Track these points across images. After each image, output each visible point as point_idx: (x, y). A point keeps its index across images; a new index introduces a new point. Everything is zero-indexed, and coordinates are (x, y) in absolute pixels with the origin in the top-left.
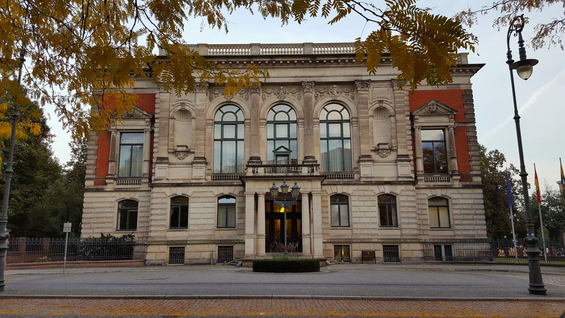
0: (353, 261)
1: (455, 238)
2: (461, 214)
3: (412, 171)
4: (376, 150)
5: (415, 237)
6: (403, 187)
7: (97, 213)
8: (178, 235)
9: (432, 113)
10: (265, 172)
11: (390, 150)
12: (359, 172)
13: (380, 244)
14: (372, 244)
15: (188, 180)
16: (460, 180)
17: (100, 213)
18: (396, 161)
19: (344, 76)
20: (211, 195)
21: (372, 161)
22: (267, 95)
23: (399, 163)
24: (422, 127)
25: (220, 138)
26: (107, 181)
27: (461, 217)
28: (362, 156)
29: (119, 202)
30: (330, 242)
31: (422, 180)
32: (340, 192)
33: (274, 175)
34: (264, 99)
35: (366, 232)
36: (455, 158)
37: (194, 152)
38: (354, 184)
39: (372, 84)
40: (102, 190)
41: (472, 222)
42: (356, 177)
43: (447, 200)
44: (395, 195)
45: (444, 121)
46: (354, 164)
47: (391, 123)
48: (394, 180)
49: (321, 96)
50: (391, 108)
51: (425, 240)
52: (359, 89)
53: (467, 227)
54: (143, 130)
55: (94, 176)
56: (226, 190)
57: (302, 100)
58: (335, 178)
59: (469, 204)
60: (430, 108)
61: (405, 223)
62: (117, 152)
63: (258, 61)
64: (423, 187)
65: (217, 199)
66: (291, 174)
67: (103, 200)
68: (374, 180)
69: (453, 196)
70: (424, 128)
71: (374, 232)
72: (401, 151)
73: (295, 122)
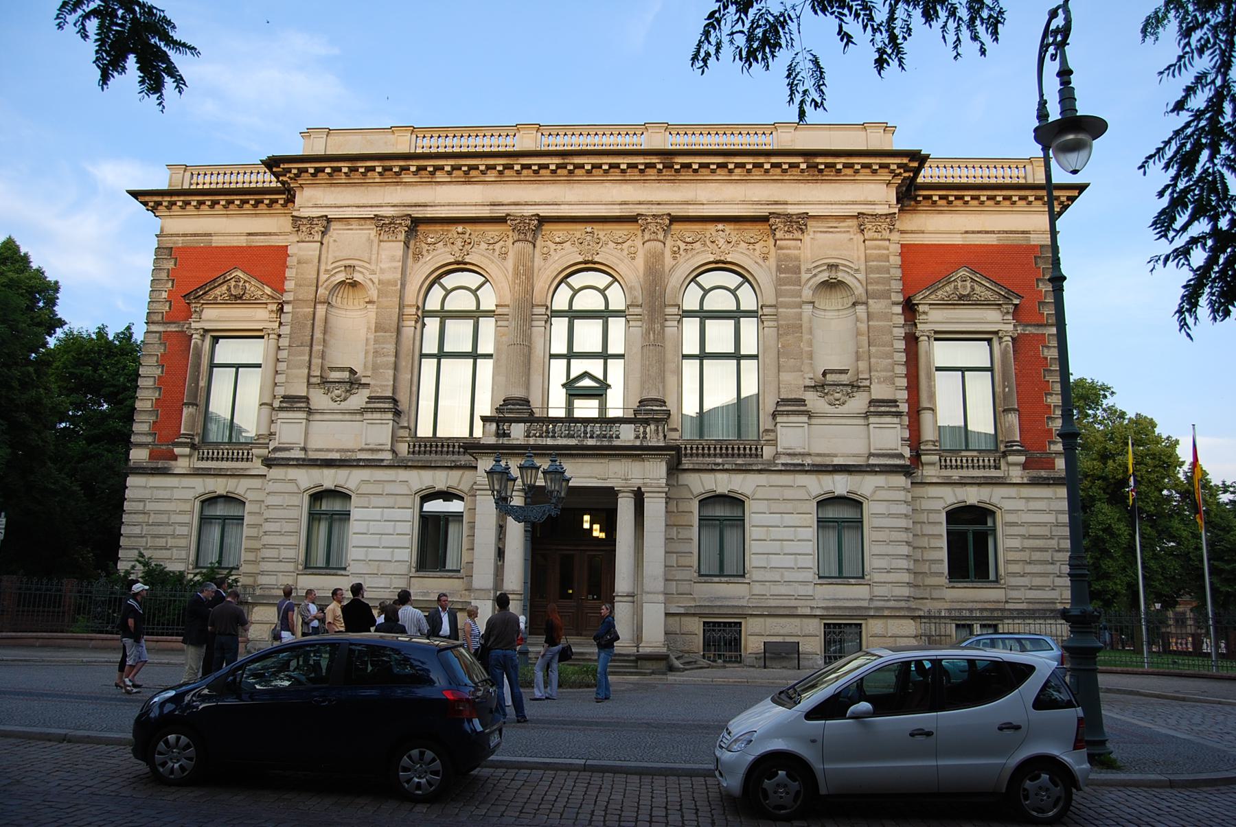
0: (748, 661)
1: (1007, 606)
2: (1023, 549)
3: (903, 439)
4: (820, 387)
5: (903, 604)
6: (880, 480)
9: (964, 301)
10: (528, 436)
11: (853, 386)
12: (774, 442)
13: (817, 620)
14: (797, 621)
15: (353, 451)
16: (1025, 466)
18: (867, 415)
20: (291, 487)
21: (809, 414)
23: (872, 420)
24: (936, 332)
25: (565, 351)
26: (177, 450)
27: (1025, 556)
28: (783, 400)
29: (203, 502)
30: (694, 615)
31: (933, 464)
32: (722, 489)
33: (550, 442)
35: (783, 590)
36: (1014, 410)
37: (367, 385)
38: (760, 471)
39: (810, 223)
40: (164, 472)
41: (1050, 568)
42: (768, 452)
44: (860, 499)
45: (991, 319)
46: (765, 422)
47: (857, 320)
48: (861, 461)
50: (858, 285)
51: (929, 611)
52: (779, 235)
53: (1038, 581)
54: (261, 330)
55: (150, 439)
56: (440, 479)
58: (715, 455)
59: (1045, 524)
60: (956, 288)
61: (880, 570)
62: (202, 383)
63: (818, 164)
65: (418, 500)
66: (591, 442)
67: (167, 494)
68: (808, 461)
69: (1007, 505)
70: (942, 336)
71: (803, 590)
72: (880, 391)
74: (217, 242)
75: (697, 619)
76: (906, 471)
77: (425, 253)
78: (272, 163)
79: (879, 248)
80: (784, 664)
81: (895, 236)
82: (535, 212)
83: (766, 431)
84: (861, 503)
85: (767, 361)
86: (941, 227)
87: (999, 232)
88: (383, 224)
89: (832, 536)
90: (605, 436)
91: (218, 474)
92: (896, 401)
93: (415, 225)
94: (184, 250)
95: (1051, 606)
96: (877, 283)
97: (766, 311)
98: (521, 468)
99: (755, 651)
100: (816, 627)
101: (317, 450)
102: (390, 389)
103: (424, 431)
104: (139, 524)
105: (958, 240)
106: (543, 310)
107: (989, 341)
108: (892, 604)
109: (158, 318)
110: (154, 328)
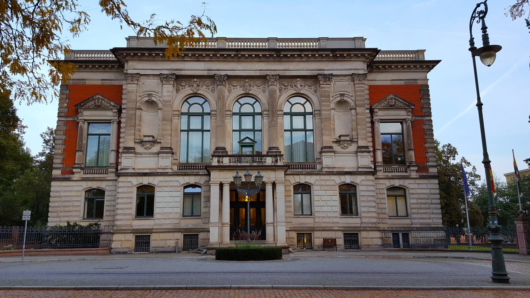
1: (412, 226)
2: (418, 203)
4: (338, 142)
5: (374, 225)
6: (363, 177)
7: (64, 201)
8: (352, 222)
9: (391, 107)
10: (230, 162)
11: (351, 141)
12: (321, 163)
14: (333, 232)
15: (155, 169)
16: (417, 171)
17: (67, 201)
18: (357, 152)
19: (307, 70)
20: (333, 183)
22: (232, 87)
23: (359, 154)
24: (381, 120)
26: (74, 170)
29: (86, 192)
30: (293, 230)
31: (381, 171)
32: (303, 181)
33: (239, 164)
34: (230, 91)
35: (327, 220)
37: (160, 143)
38: (317, 174)
40: (69, 180)
41: (428, 211)
42: (318, 167)
43: (405, 190)
45: (402, 114)
46: (317, 155)
48: (354, 170)
49: (285, 89)
52: (321, 83)
54: (110, 120)
55: (61, 166)
56: (192, 180)
57: (267, 93)
58: (298, 168)
60: (389, 102)
61: (365, 212)
64: (382, 177)
65: (183, 188)
66: (255, 164)
67: (70, 189)
69: (410, 186)
70: (383, 121)
72: (361, 143)
73: (260, 114)
74: (88, 83)
75: (294, 232)
76: (373, 173)
77: (232, 90)
78: (115, 51)
79: (361, 87)
80: (329, 249)
81: (366, 82)
82: (226, 73)
83: (318, 159)
84: (356, 186)
85: (317, 132)
86: (383, 79)
87: (405, 80)
88: (163, 78)
89: (189, 201)
90: (260, 162)
91: (93, 180)
92: (368, 147)
93: (179, 79)
94: (73, 86)
95: (430, 226)
96: (360, 101)
97: (316, 112)
98: (245, 175)
99: (318, 244)
100: (341, 235)
101: (139, 169)
102: (170, 144)
103: (183, 160)
104: (57, 202)
105: (389, 83)
106: (177, 113)
107: (402, 123)
108: (370, 225)
109: (63, 115)
110: (427, 118)
